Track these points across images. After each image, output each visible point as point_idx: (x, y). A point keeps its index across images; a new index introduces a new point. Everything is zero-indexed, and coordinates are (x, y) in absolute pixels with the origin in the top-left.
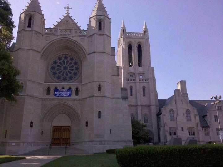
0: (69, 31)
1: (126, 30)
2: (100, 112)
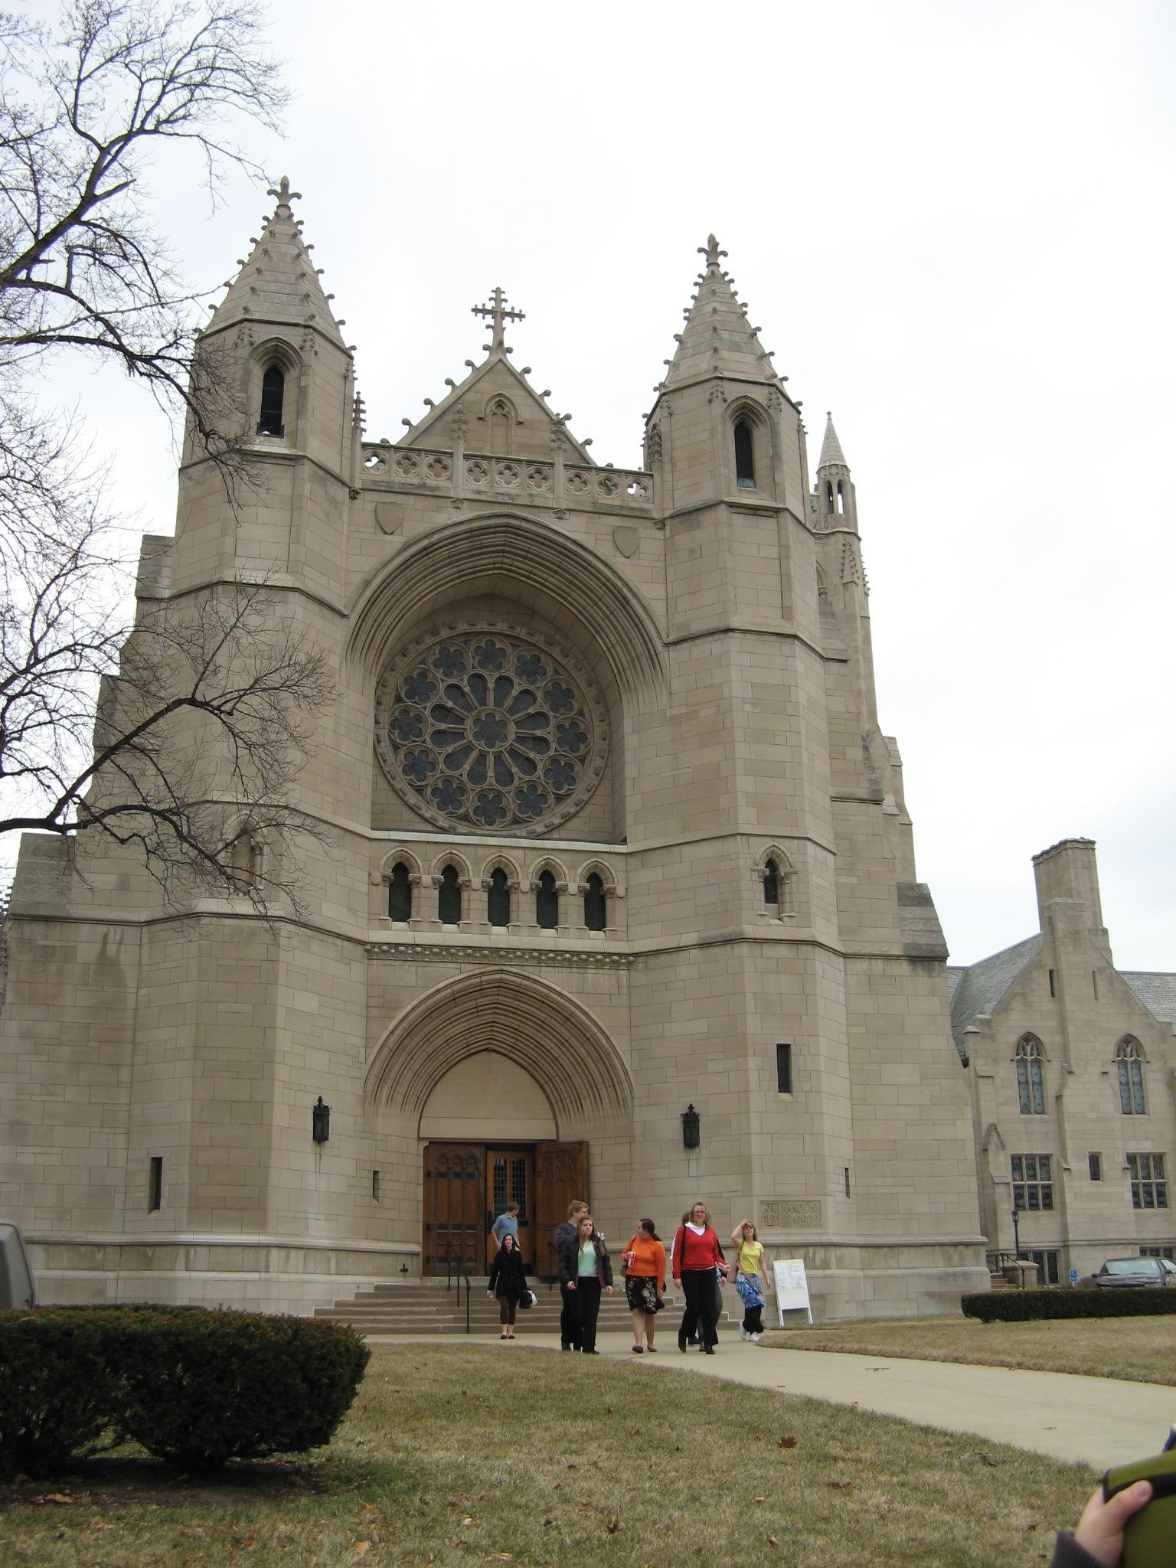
0: (431, 459)
2: (784, 1051)
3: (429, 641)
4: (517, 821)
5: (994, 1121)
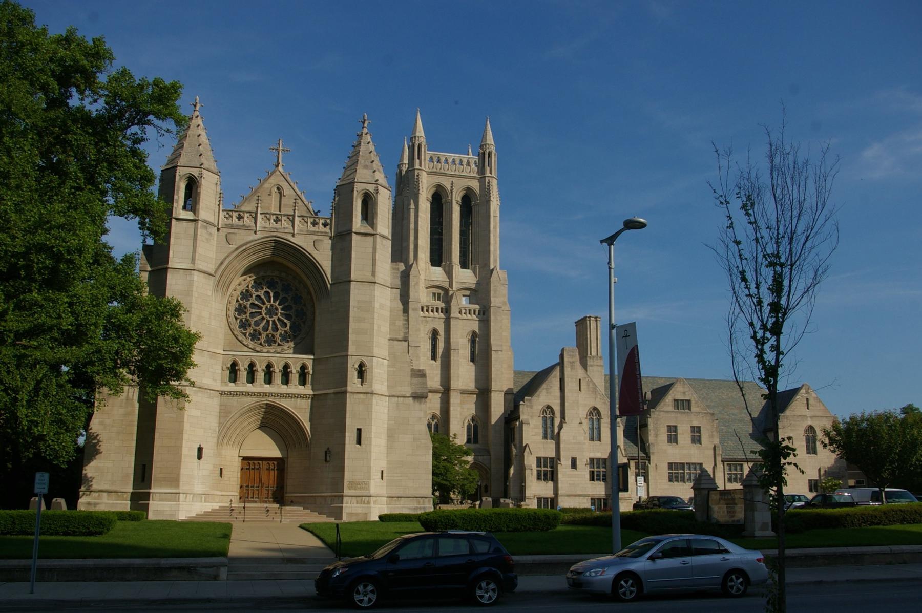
2: (359, 430)
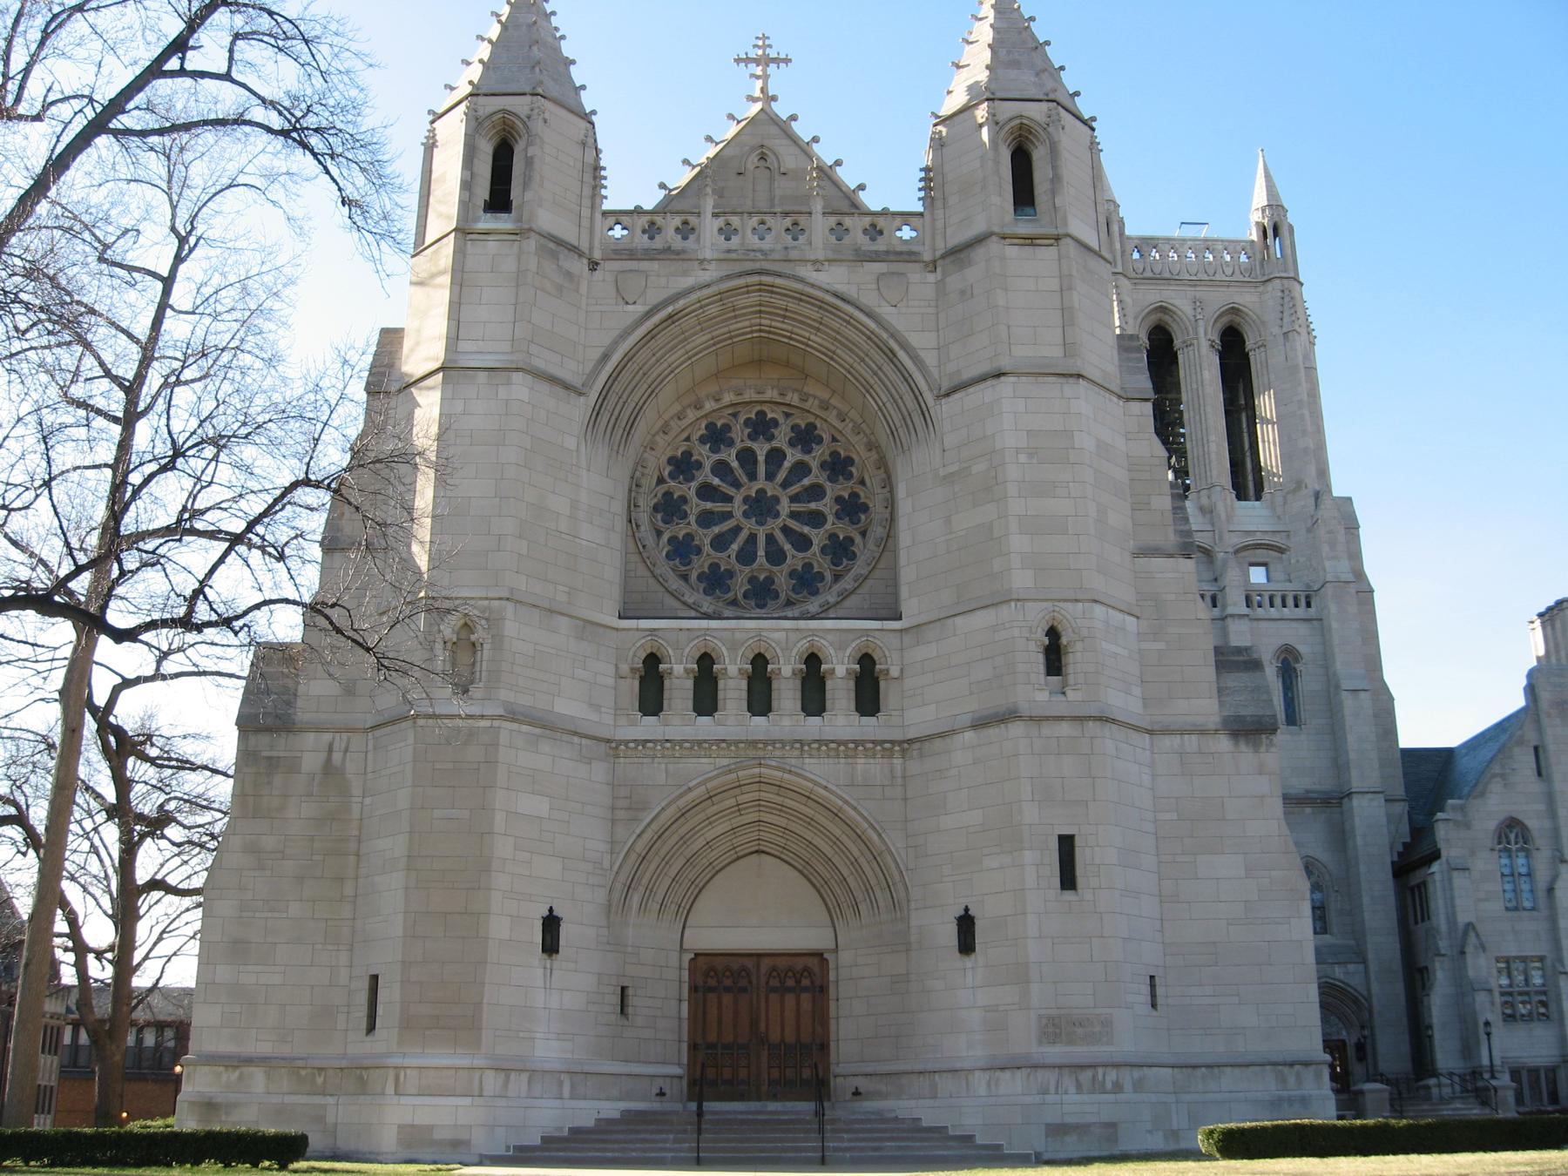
0: (788, 222)
1: (1121, 223)
2: (1067, 845)
3: (692, 415)
4: (789, 603)
5: (1473, 920)
